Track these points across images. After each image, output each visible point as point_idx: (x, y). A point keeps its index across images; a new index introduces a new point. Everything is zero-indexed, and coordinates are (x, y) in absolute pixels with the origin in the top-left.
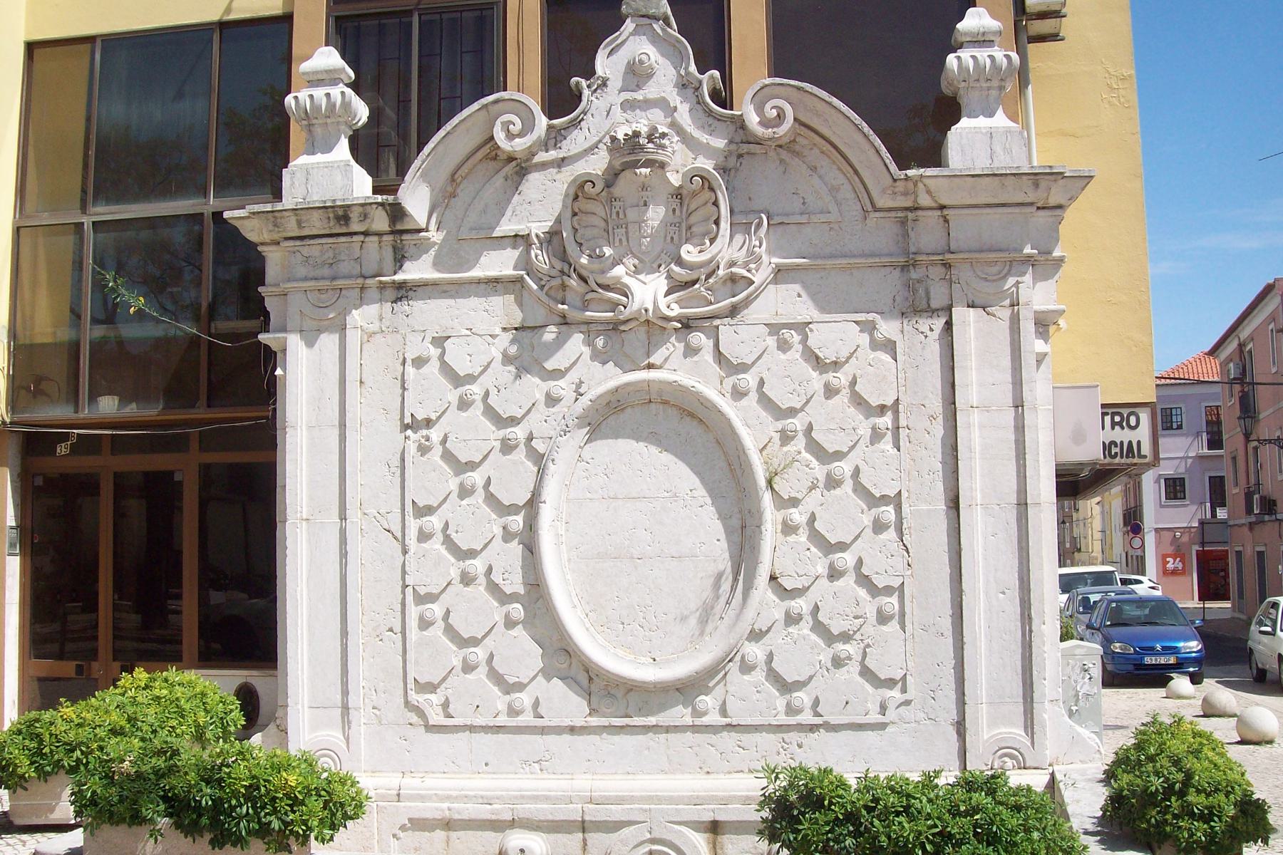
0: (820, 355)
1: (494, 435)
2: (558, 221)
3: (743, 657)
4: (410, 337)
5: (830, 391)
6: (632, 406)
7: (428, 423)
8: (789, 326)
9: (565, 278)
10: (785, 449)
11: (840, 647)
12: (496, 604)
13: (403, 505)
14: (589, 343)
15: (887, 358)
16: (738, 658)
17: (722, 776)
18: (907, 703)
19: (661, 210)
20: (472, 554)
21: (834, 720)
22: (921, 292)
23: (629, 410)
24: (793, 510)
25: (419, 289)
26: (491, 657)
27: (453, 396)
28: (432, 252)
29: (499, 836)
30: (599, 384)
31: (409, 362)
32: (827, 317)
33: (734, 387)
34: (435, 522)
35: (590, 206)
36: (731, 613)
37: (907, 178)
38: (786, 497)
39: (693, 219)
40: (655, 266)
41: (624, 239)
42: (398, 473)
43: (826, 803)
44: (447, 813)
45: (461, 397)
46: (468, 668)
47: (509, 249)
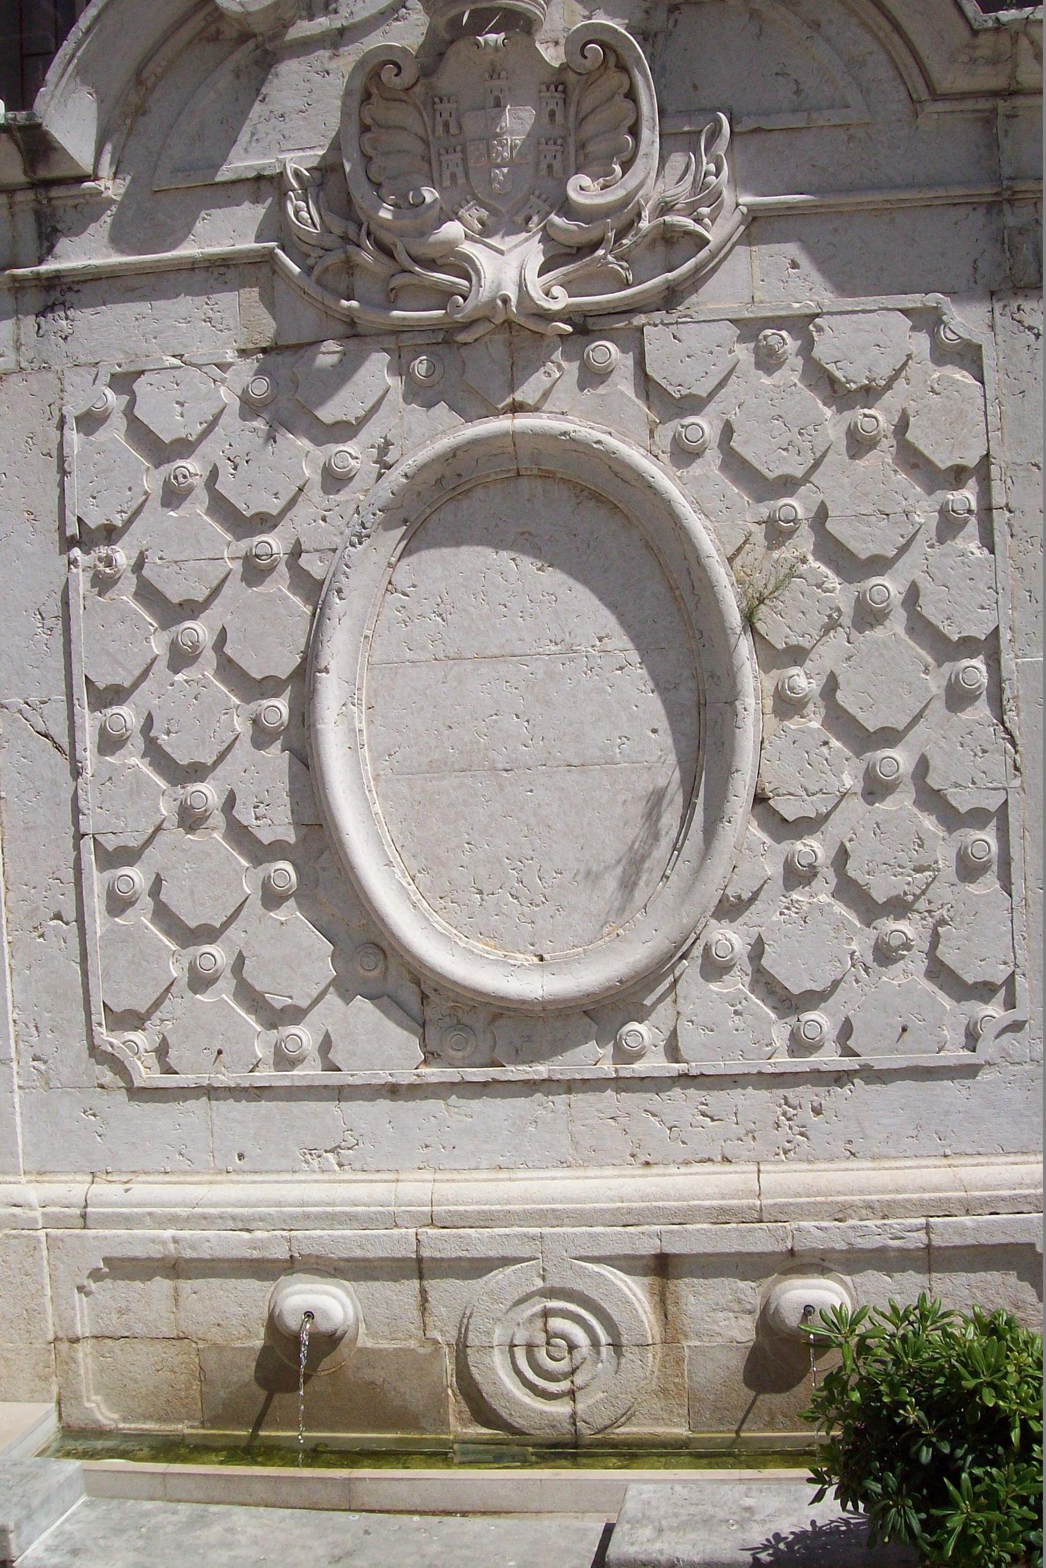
0: (839, 374)
1: (227, 549)
2: (336, 146)
3: (707, 949)
4: (72, 377)
5: (859, 444)
6: (486, 485)
7: (110, 534)
8: (777, 322)
9: (351, 248)
10: (776, 555)
11: (889, 925)
12: (245, 863)
13: (69, 686)
14: (400, 368)
15: (963, 377)
16: (698, 951)
17: (673, 1169)
18: (1016, 1026)
19: (528, 115)
20: (198, 772)
21: (881, 1061)
22: (1026, 250)
23: (479, 493)
24: (794, 670)
25: (85, 289)
26: (240, 961)
27: (151, 482)
28: (107, 218)
29: (269, 1286)
30: (422, 445)
31: (71, 422)
32: (849, 303)
33: (676, 441)
34: (127, 715)
35: (397, 114)
36: (683, 867)
37: (1000, 27)
38: (781, 646)
39: (589, 128)
40: (519, 219)
41: (459, 171)
42: (59, 629)
43: (1015, 1435)
44: (172, 1247)
45: (167, 483)
46: (200, 981)
47: (247, 205)
